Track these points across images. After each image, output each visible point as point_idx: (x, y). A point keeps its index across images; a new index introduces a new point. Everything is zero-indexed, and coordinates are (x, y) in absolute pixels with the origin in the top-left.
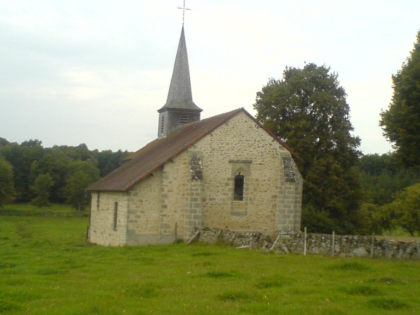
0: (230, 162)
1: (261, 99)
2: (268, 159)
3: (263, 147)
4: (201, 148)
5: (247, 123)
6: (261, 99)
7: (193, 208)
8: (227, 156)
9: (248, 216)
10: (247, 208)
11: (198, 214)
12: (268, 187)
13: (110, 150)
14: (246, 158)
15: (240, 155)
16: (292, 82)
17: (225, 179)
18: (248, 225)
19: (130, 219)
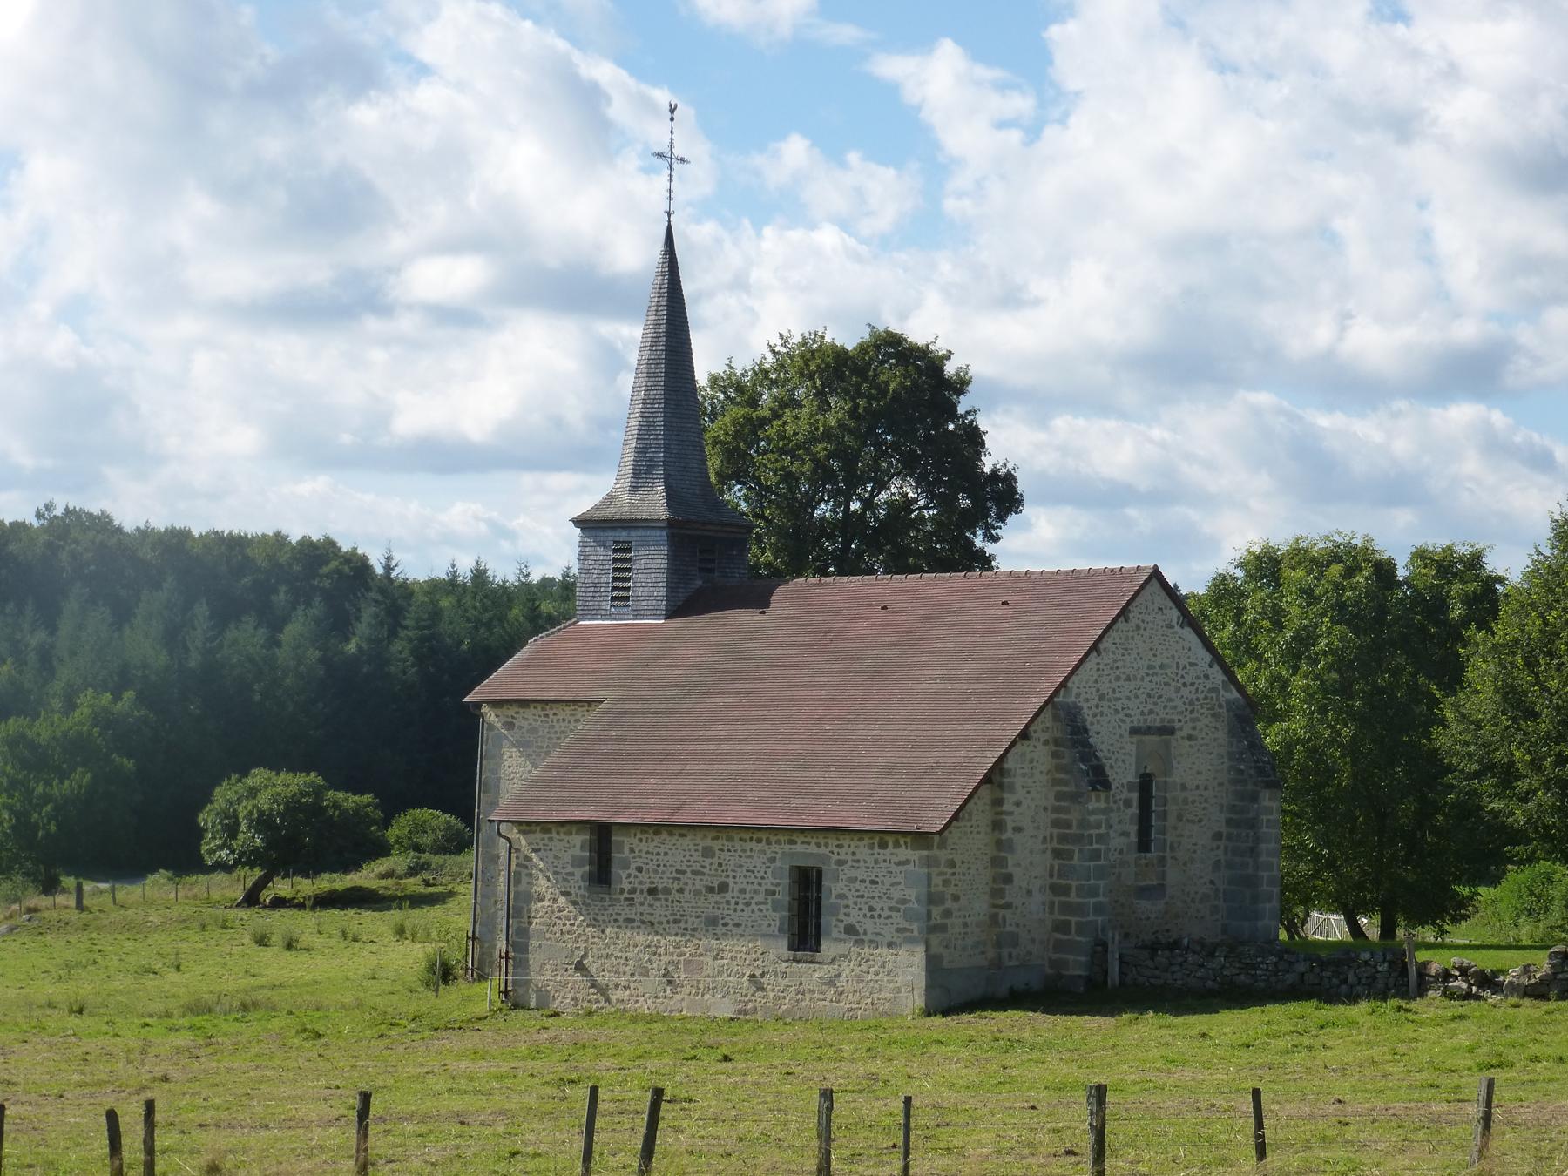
0: (1135, 731)
1: (1413, 706)
2: (1205, 721)
3: (1193, 684)
4: (1078, 695)
5: (1163, 614)
6: (1413, 706)
7: (1092, 882)
8: (1127, 715)
9: (840, 868)
10: (1163, 876)
11: (1101, 899)
12: (1204, 809)
13: (304, 537)
14: (1162, 720)
15: (1151, 712)
16: (1341, 575)
17: (1123, 785)
18: (1167, 927)
19: (933, 922)
